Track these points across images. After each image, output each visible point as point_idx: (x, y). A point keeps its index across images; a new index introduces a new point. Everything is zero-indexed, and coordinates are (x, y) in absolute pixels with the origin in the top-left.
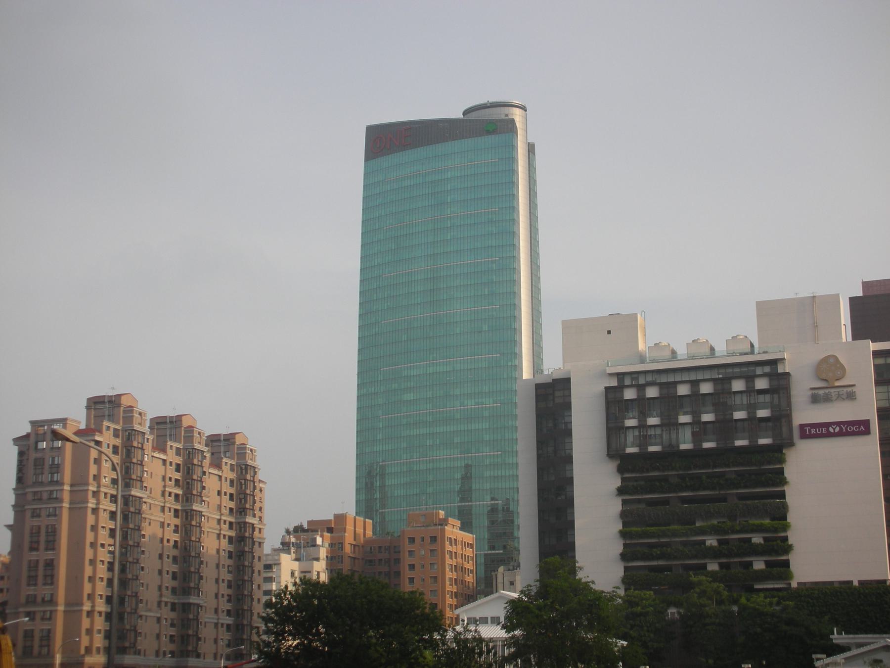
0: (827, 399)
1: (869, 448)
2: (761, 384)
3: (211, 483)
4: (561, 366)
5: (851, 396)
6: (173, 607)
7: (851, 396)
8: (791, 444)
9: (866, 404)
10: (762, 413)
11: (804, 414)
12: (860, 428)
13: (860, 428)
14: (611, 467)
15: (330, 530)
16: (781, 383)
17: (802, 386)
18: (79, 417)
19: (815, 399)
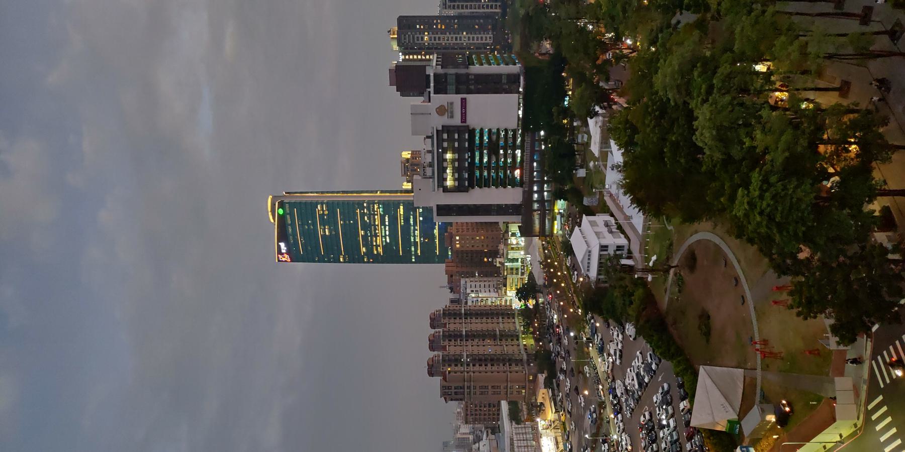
0: (452, 112)
1: (471, 98)
2: (445, 136)
3: (452, 327)
4: (850, 379)
5: (452, 104)
6: (501, 340)
7: (452, 104)
8: (468, 126)
9: (456, 98)
10: (456, 136)
11: (457, 121)
12: (464, 102)
13: (464, 102)
14: (472, 191)
15: (452, 276)
16: (446, 129)
17: (445, 120)
18: (437, 380)
19: (452, 117)
